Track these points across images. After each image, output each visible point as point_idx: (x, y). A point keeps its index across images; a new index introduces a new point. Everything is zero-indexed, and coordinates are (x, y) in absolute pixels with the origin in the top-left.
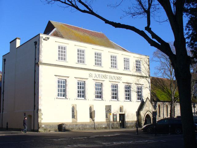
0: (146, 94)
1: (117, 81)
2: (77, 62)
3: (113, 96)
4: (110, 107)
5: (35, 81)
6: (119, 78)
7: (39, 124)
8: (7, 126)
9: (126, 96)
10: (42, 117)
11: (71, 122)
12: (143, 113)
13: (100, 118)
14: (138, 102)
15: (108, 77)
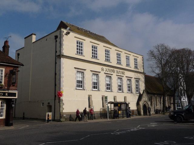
0: (142, 87)
1: (122, 75)
2: (76, 53)
3: (78, 84)
4: (106, 98)
5: (56, 72)
6: (123, 73)
7: (61, 114)
8: (24, 116)
9: (107, 87)
10: (64, 107)
11: (94, 111)
12: (141, 103)
13: (97, 107)
14: (128, 93)
15: (115, 71)
